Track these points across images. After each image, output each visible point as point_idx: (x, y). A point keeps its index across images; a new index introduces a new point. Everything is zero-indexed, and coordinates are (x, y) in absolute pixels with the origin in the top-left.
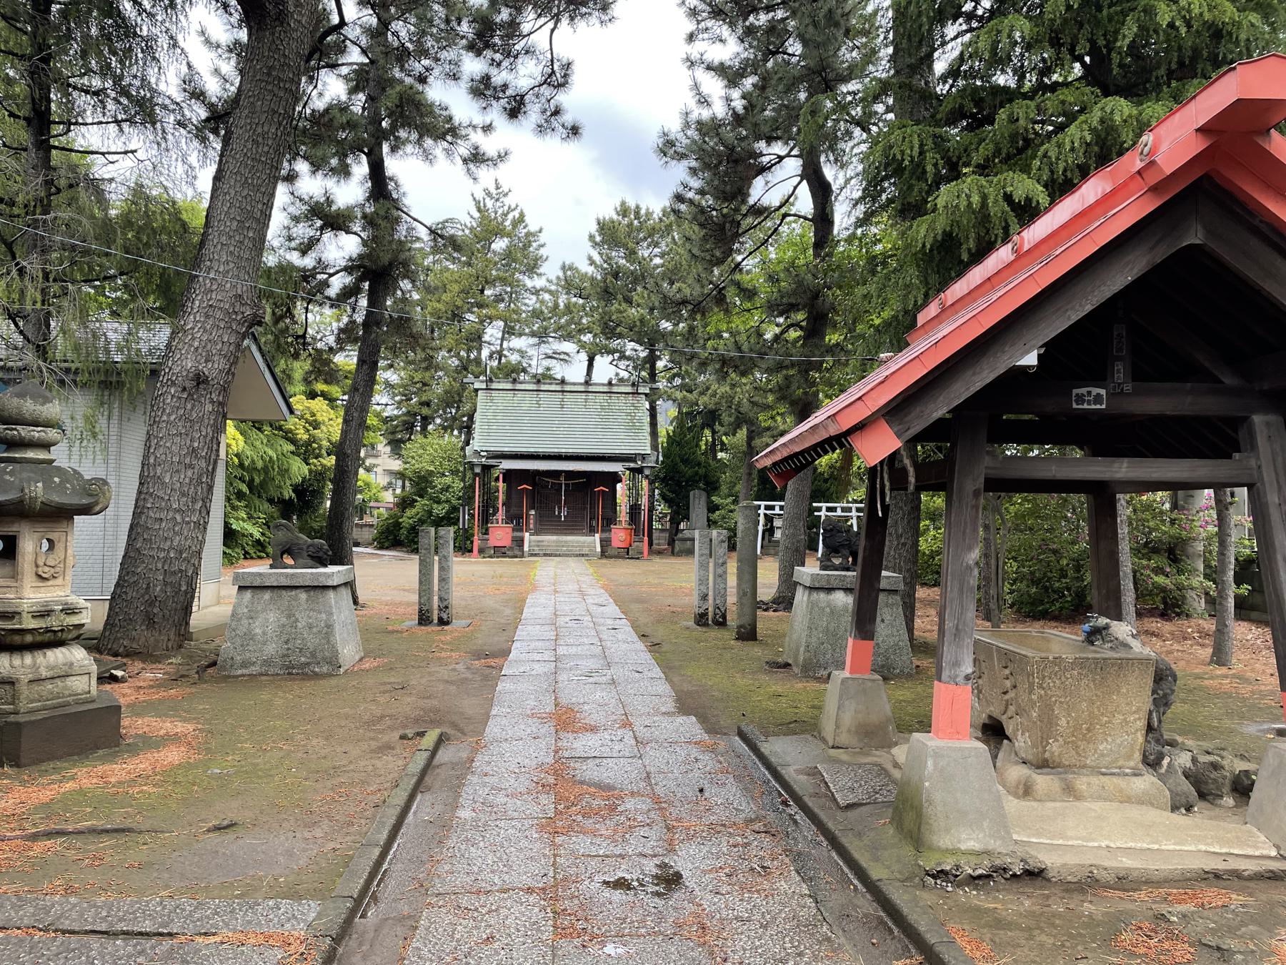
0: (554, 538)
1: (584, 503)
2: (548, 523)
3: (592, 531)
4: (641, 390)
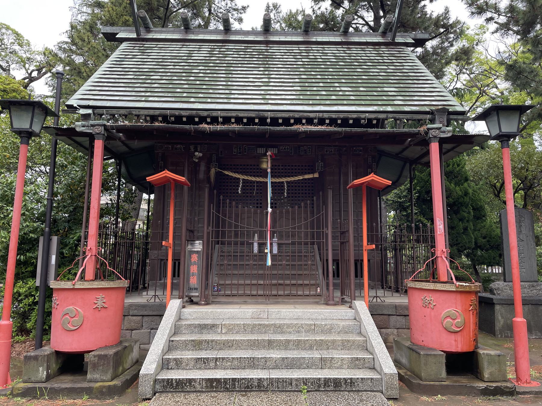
1: (318, 224)
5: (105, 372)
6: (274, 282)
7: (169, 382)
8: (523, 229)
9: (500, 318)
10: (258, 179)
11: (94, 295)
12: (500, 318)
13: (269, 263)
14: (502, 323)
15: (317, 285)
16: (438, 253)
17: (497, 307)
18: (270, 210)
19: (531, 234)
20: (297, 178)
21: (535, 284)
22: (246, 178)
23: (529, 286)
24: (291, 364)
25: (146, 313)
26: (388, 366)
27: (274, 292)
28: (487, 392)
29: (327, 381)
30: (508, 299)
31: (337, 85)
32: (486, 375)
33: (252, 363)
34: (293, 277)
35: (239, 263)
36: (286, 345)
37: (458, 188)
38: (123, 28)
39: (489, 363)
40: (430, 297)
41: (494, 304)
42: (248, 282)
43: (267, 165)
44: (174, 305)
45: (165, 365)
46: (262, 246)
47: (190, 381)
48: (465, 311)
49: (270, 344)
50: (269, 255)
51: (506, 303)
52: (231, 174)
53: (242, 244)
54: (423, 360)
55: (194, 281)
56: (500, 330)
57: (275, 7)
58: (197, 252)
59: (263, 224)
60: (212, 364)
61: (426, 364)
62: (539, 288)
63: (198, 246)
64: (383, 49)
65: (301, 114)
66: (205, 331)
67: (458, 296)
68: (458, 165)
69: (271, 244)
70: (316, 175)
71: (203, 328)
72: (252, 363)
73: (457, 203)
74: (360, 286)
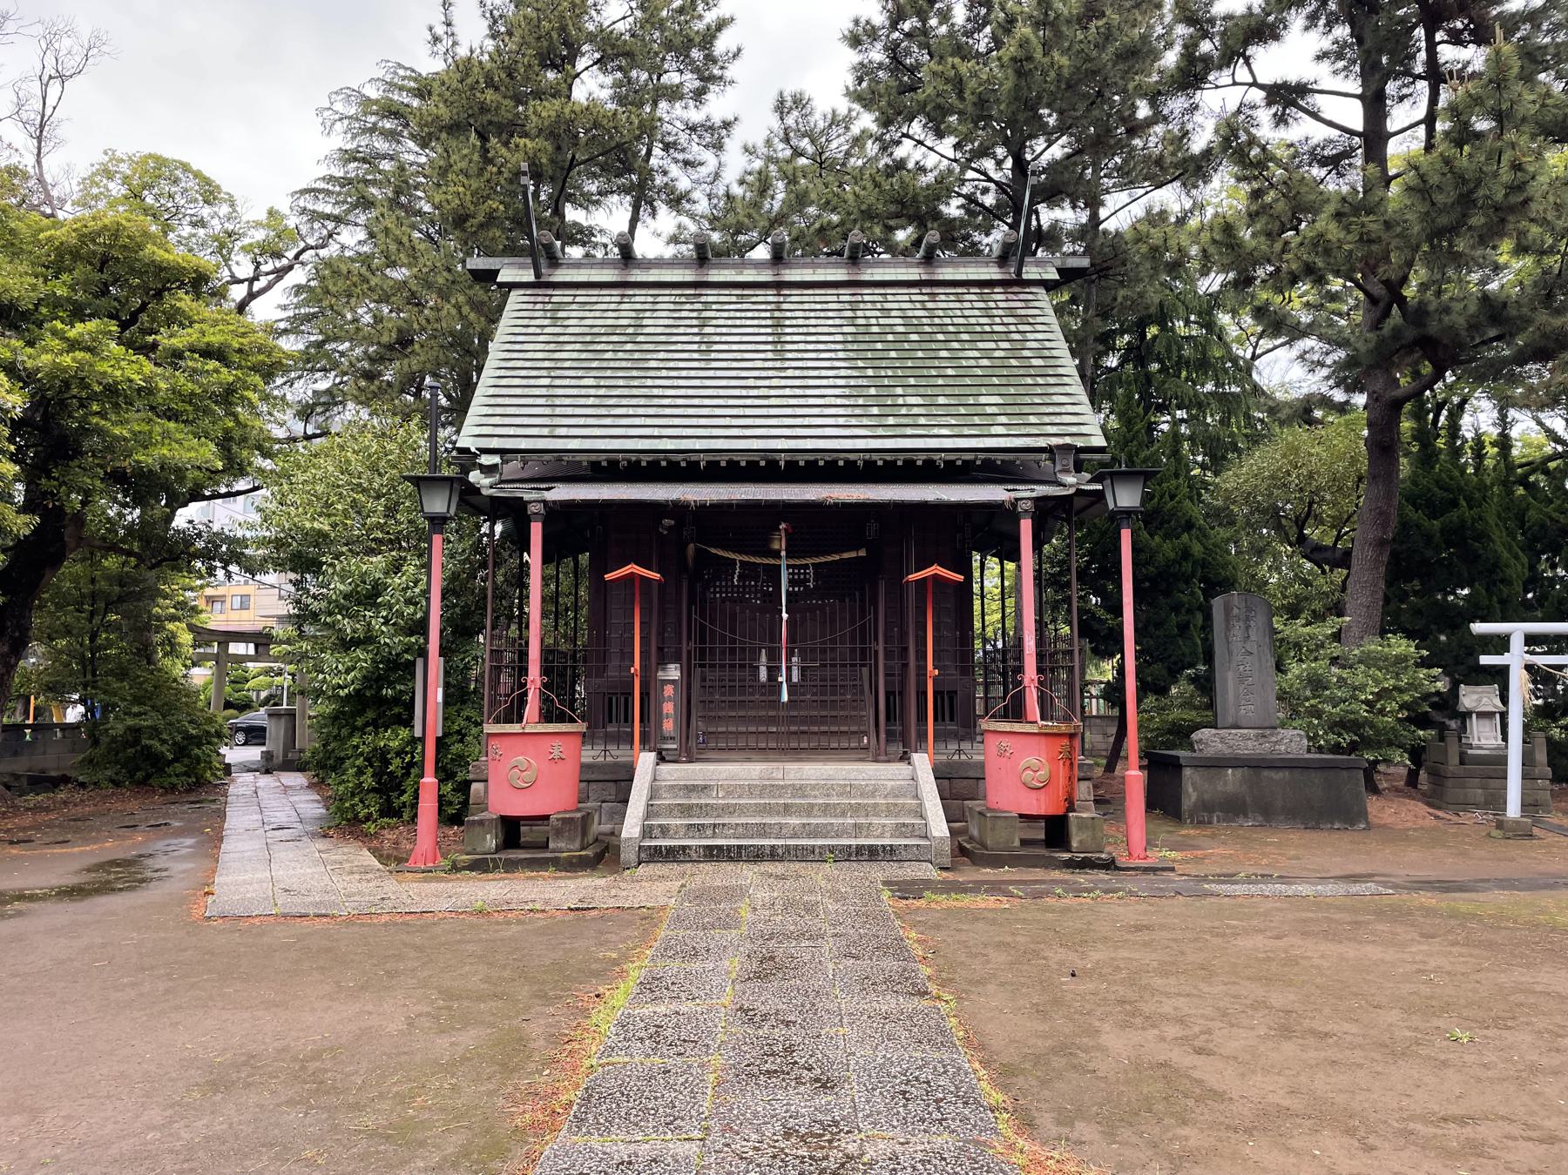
0: (750, 771)
1: (864, 635)
2: (728, 714)
3: (897, 738)
4: (1030, 273)
5: (571, 840)
6: (793, 728)
7: (657, 849)
10: (766, 561)
11: (548, 741)
13: (785, 697)
15: (866, 733)
16: (1026, 682)
17: (1187, 772)
18: (785, 616)
20: (830, 559)
21: (1268, 732)
22: (746, 559)
23: (1257, 736)
24: (815, 832)
25: (593, 777)
26: (939, 827)
27: (794, 745)
28: (1070, 865)
29: (860, 849)
31: (899, 391)
32: (1074, 844)
33: (763, 830)
34: (823, 720)
35: (738, 698)
36: (809, 810)
37: (1167, 546)
38: (506, 260)
39: (1080, 828)
40: (1006, 742)
42: (752, 729)
43: (780, 544)
44: (645, 761)
45: (647, 832)
46: (773, 671)
47: (684, 848)
48: (1051, 760)
49: (787, 809)
50: (785, 686)
52: (721, 553)
53: (742, 666)
54: (989, 825)
55: (669, 726)
57: (799, 102)
58: (673, 682)
59: (774, 636)
60: (709, 832)
61: (993, 829)
63: (673, 672)
64: (998, 295)
65: (835, 455)
66: (694, 795)
67: (1043, 740)
68: (1172, 497)
69: (789, 669)
70: (862, 553)
71: (691, 789)
72: (763, 830)
74: (922, 736)
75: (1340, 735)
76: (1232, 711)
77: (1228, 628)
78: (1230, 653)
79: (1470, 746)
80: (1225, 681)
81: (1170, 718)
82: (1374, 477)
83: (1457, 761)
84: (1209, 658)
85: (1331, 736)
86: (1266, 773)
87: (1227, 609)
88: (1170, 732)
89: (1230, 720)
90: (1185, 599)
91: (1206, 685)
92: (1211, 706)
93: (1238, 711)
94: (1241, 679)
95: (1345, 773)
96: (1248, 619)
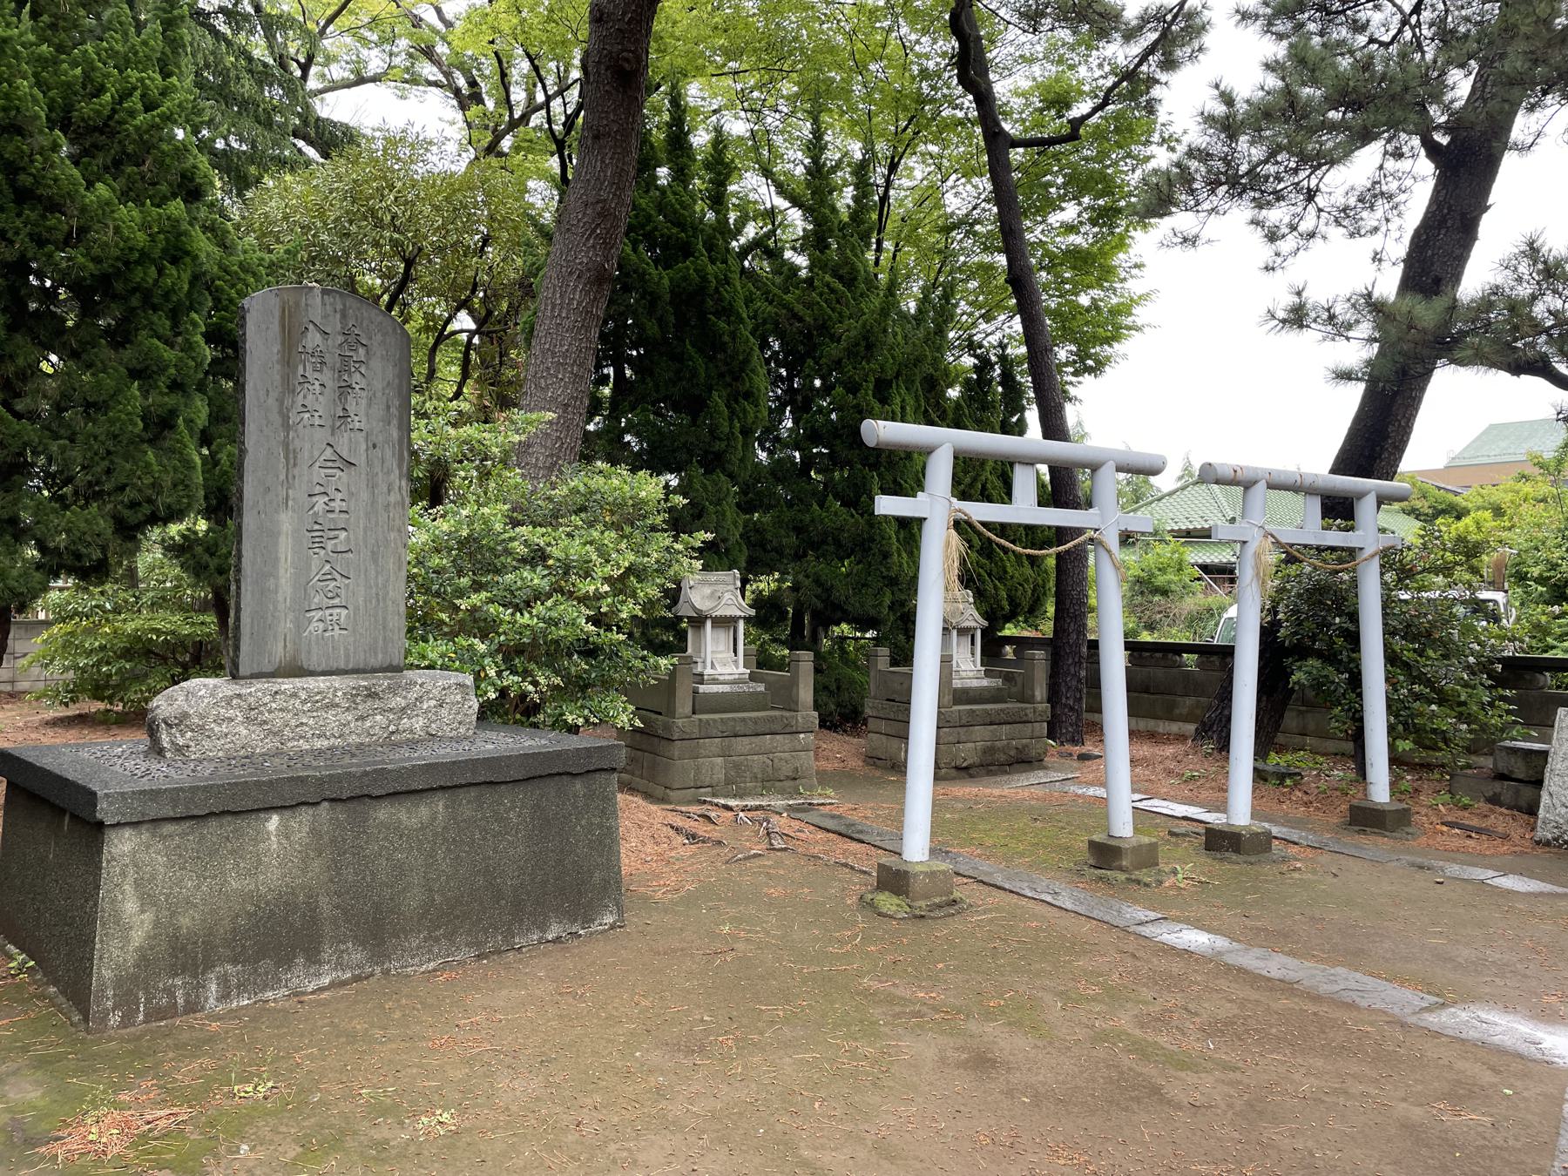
8: (356, 405)
9: (130, 906)
12: (130, 906)
14: (138, 937)
17: (122, 846)
19: (395, 434)
21: (383, 681)
23: (352, 697)
30: (194, 790)
37: (128, 213)
41: (100, 826)
51: (180, 811)
56: (119, 982)
62: (399, 701)
73: (119, 286)
75: (525, 674)
76: (287, 625)
77: (289, 387)
78: (291, 456)
79: (700, 678)
80: (274, 535)
81: (130, 627)
82: (596, 136)
83: (688, 709)
84: (223, 504)
85: (510, 680)
86: (383, 813)
87: (291, 333)
88: (127, 654)
89: (278, 652)
90: (169, 355)
91: (214, 569)
92: (221, 605)
93: (299, 627)
94: (318, 533)
95: (578, 786)
96: (345, 365)
